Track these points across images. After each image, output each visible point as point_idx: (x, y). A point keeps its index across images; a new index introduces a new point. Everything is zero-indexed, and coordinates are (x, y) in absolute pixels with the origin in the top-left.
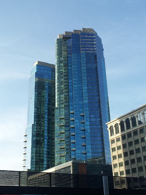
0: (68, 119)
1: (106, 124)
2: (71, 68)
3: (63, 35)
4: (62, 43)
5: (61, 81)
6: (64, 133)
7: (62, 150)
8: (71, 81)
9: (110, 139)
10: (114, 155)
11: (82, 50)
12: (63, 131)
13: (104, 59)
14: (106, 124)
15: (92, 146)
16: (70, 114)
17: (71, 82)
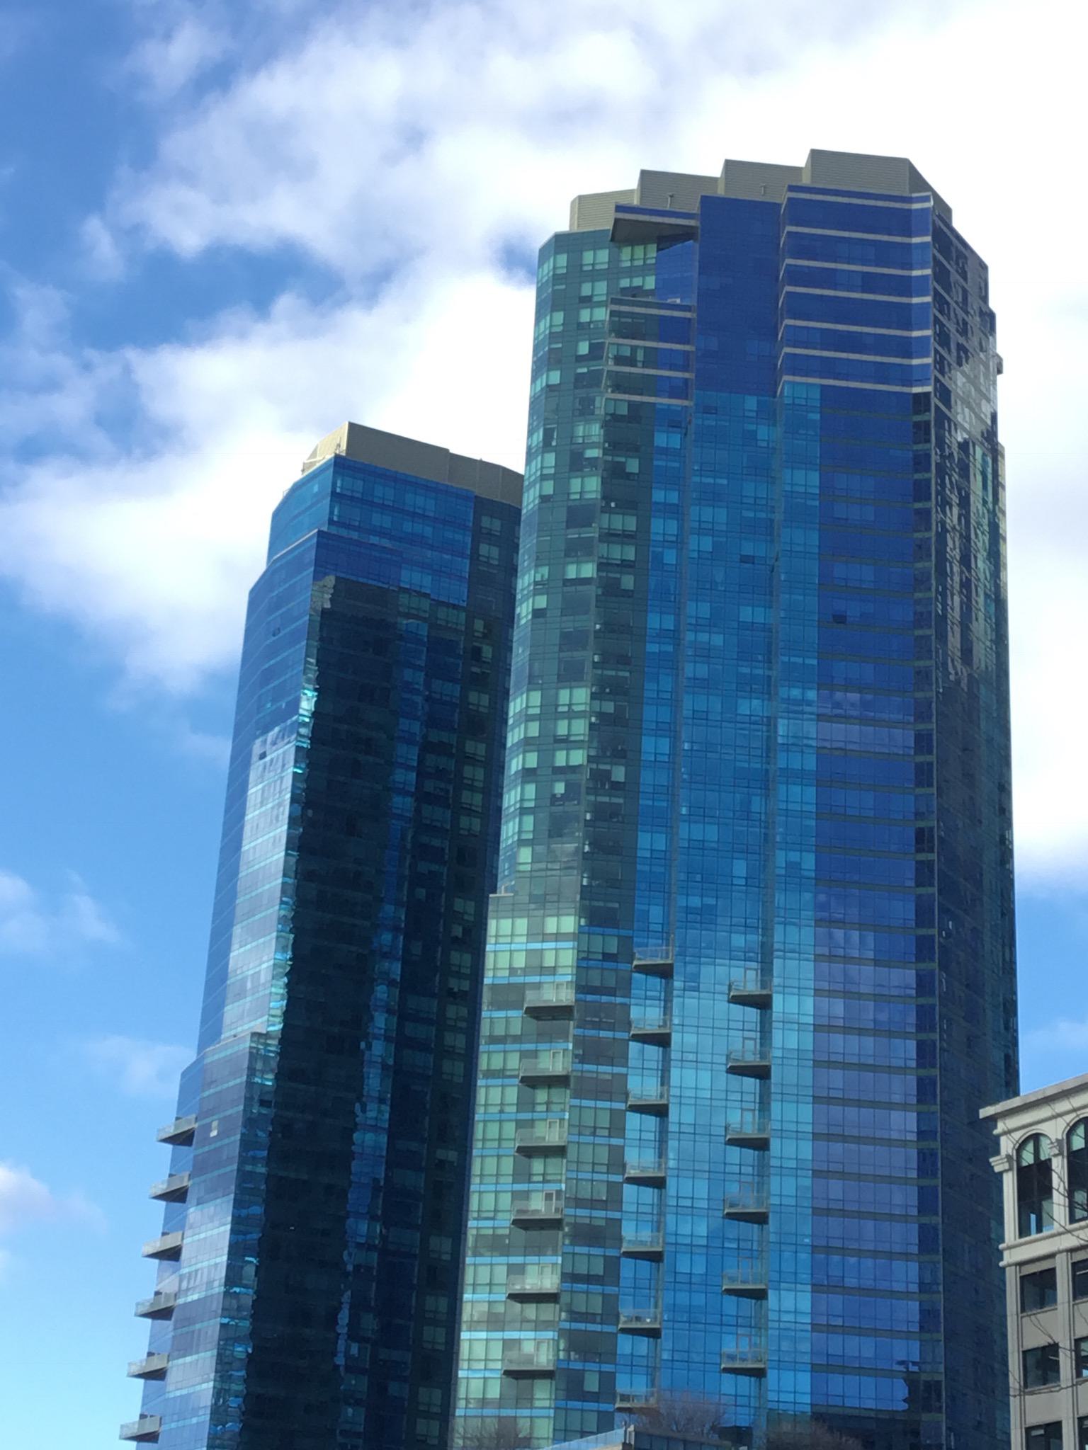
0: (598, 1269)
1: (985, 1112)
2: (673, 526)
3: (619, 208)
4: (573, 534)
5: (568, 582)
6: (560, 1151)
7: (531, 1310)
8: (669, 622)
9: (1009, 1258)
10: (1035, 1340)
11: (799, 366)
12: (552, 1135)
13: (989, 319)
14: (985, 1112)
15: (822, 1144)
16: (629, 1191)
17: (662, 634)
